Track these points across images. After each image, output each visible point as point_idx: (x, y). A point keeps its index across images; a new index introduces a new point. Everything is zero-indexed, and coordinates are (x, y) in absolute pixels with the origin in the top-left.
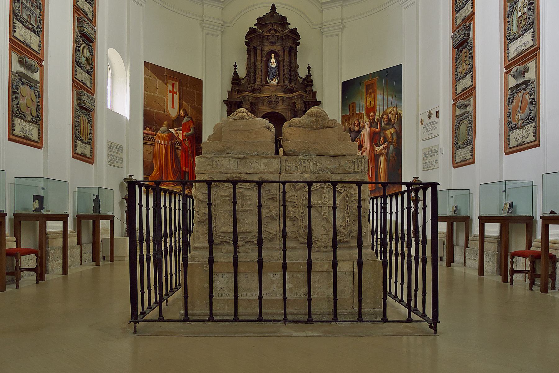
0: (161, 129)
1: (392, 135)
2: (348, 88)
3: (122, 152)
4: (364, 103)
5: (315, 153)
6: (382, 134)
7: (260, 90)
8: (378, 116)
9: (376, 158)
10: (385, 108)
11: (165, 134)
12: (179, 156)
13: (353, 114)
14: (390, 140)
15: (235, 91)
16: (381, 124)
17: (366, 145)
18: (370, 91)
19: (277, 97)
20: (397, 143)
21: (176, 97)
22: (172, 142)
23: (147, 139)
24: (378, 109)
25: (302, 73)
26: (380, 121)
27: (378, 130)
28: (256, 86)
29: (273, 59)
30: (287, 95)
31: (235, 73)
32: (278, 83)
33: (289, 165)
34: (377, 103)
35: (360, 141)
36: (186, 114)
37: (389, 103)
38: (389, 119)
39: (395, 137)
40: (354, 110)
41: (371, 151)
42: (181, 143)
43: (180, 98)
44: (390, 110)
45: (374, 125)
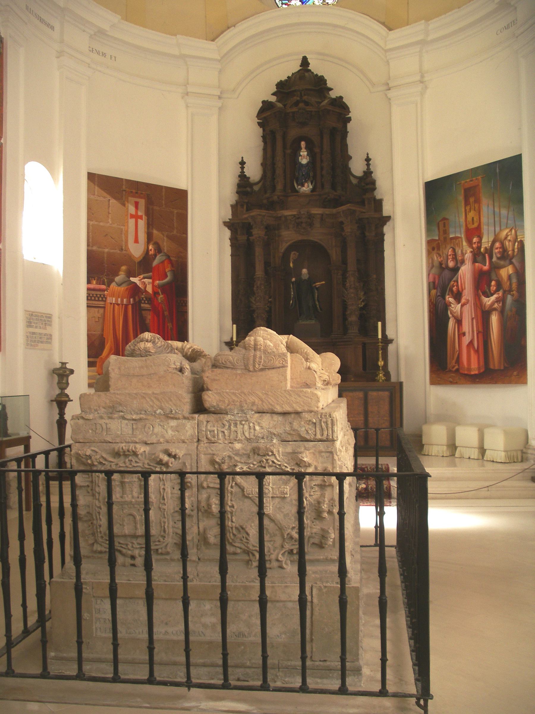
0: (117, 279)
1: (509, 277)
2: (437, 192)
3: (50, 325)
4: (462, 220)
5: (252, 410)
6: (493, 276)
7: (283, 204)
8: (486, 242)
9: (484, 316)
10: (497, 229)
11: (123, 288)
12: (148, 321)
13: (445, 239)
14: (506, 286)
15: (242, 206)
16: (491, 258)
17: (468, 294)
18: (472, 200)
19: (311, 216)
20: (518, 292)
21: (142, 223)
22: (134, 300)
23: (94, 298)
24: (484, 228)
25: (357, 167)
26: (490, 251)
27: (486, 268)
28: (275, 198)
29: (303, 150)
30: (327, 211)
31: (243, 177)
32: (313, 190)
33: (212, 429)
34: (484, 220)
35: (457, 286)
36: (159, 250)
37: (504, 221)
38: (504, 250)
39: (514, 280)
40: (445, 232)
41: (475, 304)
42: (150, 300)
43: (149, 225)
44: (504, 233)
45: (479, 258)
